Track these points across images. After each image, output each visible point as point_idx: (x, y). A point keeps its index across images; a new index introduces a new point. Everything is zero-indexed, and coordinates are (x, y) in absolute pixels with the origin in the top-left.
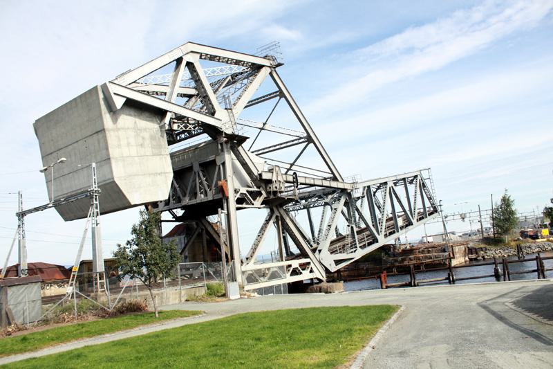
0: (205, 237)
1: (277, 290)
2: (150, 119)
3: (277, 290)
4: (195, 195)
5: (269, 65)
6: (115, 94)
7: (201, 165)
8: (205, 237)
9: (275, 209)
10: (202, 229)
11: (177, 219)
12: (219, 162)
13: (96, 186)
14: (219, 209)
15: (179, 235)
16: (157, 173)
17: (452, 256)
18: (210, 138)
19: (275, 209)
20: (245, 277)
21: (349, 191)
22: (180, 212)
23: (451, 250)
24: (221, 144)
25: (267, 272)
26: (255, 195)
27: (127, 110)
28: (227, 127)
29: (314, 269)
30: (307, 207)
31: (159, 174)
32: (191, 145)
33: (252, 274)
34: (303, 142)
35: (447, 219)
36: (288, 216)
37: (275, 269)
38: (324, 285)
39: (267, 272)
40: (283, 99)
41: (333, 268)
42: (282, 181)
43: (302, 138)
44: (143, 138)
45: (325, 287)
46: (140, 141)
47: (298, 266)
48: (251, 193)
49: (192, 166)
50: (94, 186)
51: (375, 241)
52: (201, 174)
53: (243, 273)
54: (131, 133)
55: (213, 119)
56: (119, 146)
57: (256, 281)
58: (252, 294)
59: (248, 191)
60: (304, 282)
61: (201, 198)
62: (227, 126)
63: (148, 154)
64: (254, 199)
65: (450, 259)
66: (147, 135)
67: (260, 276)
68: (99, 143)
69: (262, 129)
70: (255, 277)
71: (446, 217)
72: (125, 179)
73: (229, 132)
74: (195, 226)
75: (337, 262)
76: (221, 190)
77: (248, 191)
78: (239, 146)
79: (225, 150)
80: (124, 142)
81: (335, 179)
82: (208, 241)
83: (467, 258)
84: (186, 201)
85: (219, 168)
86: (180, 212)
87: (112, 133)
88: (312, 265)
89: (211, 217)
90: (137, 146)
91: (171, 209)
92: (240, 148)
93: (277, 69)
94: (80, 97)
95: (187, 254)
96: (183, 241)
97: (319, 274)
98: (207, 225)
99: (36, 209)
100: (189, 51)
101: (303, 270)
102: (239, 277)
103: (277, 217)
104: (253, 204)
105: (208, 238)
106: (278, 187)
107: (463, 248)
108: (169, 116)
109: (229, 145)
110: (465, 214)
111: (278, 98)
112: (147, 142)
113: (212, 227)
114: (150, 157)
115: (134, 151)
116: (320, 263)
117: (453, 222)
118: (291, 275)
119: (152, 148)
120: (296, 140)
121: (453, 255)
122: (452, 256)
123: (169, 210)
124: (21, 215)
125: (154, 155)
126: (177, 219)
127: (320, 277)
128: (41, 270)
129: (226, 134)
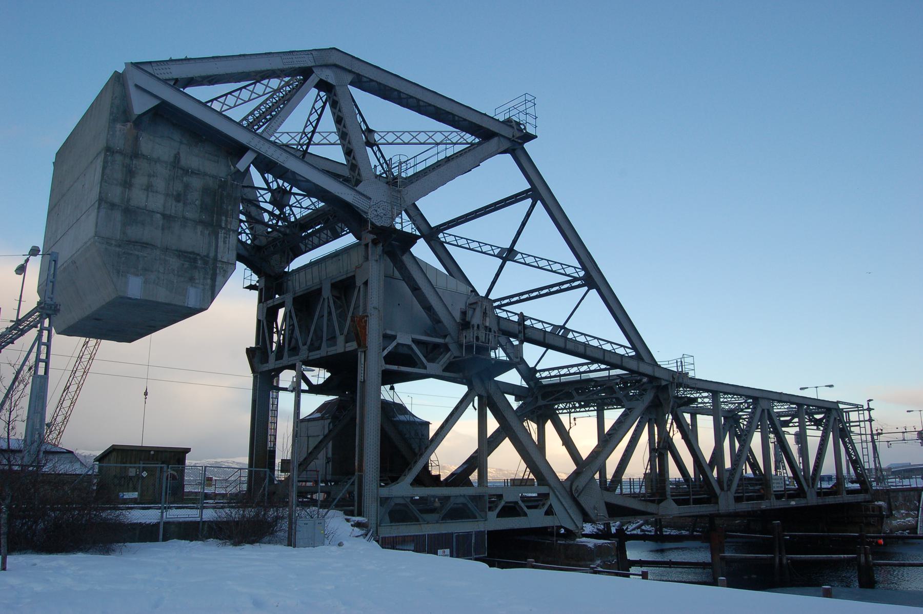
5: (510, 136)
6: (137, 86)
12: (359, 282)
21: (664, 383)
28: (380, 211)
29: (557, 507)
36: (297, 293)
37: (462, 500)
46: (179, 187)
52: (331, 302)
53: (383, 501)
55: (353, 193)
63: (188, 215)
67: (422, 511)
77: (414, 341)
80: (140, 180)
88: (552, 500)
90: (167, 195)
92: (405, 258)
101: (529, 507)
109: (380, 248)
112: (195, 196)
118: (500, 515)
125: (201, 222)
128: (284, 71)
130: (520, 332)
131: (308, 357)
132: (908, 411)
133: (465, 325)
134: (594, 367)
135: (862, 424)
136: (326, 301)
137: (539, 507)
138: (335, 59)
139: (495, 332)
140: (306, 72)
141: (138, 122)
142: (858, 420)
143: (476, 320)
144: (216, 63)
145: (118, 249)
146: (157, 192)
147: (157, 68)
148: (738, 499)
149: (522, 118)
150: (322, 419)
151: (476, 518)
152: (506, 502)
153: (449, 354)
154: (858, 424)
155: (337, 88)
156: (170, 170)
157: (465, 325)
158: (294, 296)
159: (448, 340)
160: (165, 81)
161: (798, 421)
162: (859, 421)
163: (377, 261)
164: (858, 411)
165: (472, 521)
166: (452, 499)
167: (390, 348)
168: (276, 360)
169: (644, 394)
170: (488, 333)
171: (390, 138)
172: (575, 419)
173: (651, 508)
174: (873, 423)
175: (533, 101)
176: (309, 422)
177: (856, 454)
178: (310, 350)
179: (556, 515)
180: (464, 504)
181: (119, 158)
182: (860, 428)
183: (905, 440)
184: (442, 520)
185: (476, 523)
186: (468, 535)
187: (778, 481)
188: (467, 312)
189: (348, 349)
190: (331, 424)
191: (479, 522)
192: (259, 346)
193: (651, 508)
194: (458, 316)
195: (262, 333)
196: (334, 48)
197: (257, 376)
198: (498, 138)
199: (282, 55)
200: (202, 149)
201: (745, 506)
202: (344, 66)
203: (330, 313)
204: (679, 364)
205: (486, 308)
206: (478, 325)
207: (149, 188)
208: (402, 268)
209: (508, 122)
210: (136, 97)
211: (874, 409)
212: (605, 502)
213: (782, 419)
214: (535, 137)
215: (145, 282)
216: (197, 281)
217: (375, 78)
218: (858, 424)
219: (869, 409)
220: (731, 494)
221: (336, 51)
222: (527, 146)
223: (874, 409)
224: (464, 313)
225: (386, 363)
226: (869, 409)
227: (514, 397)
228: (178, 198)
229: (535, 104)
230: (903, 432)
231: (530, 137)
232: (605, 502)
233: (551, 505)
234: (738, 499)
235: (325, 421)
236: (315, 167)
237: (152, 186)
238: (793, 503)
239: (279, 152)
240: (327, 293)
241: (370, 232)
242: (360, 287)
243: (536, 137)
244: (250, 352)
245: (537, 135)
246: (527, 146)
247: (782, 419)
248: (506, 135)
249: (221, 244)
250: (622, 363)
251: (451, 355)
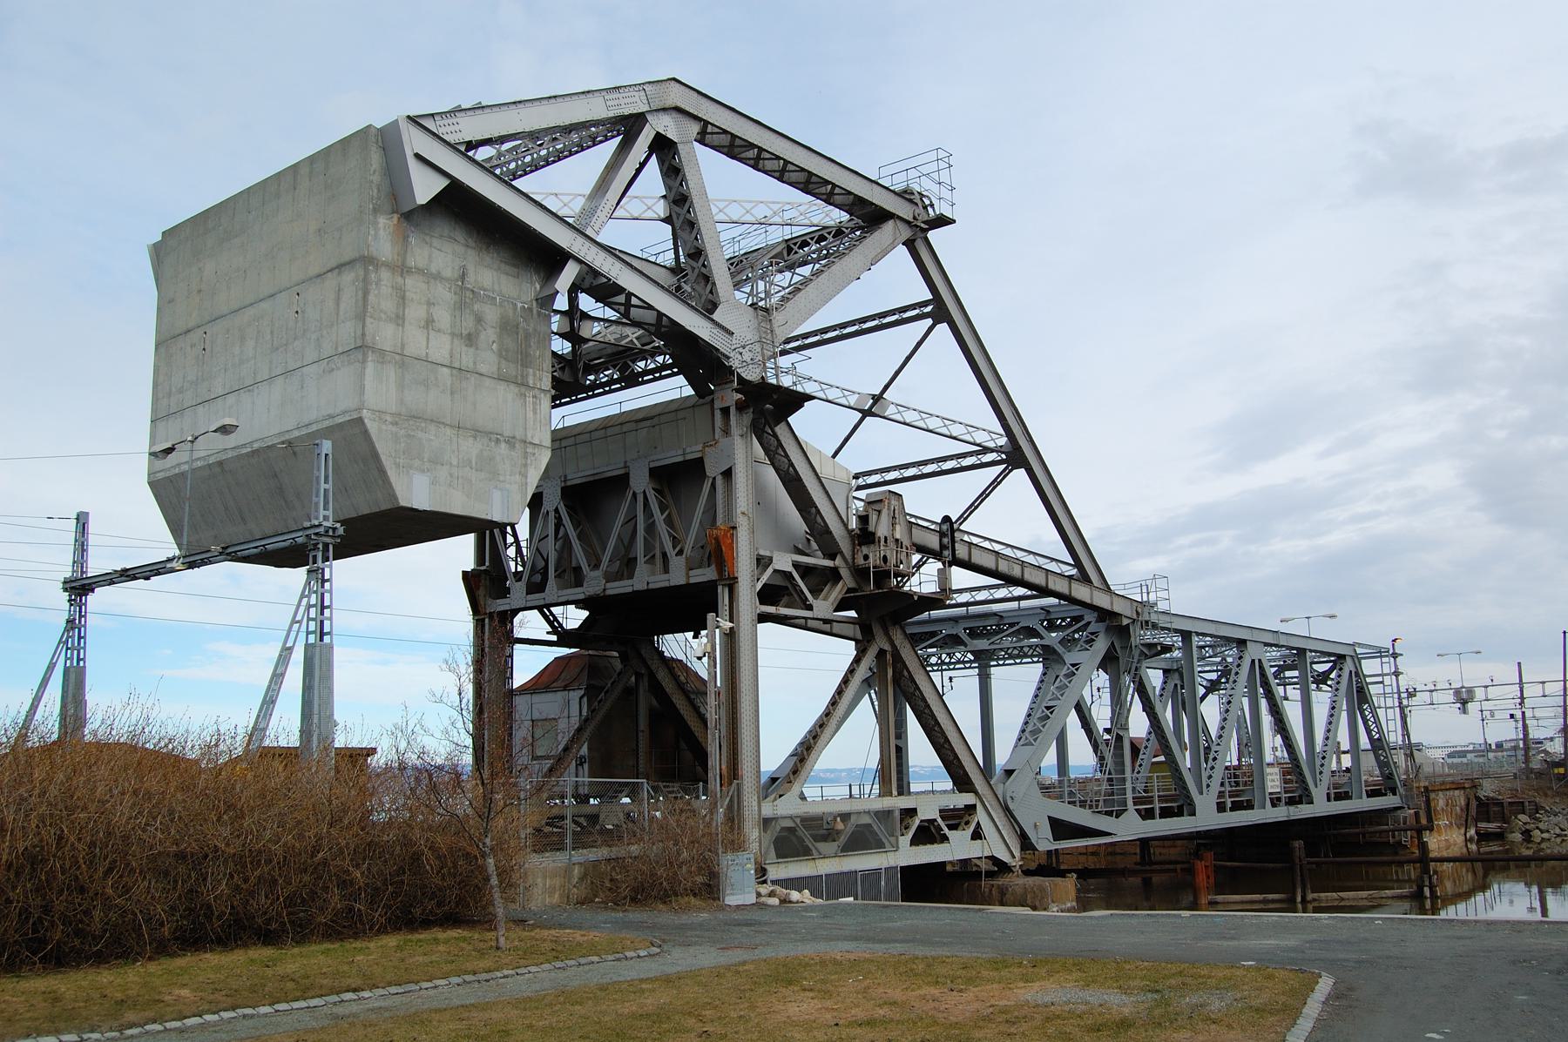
0: (645, 702)
2: (514, 270)
4: (628, 566)
6: (418, 156)
7: (656, 473)
8: (645, 702)
9: (877, 630)
10: (638, 676)
11: (564, 637)
12: (713, 469)
13: (330, 513)
14: (711, 616)
15: (565, 688)
17: (1424, 821)
19: (877, 630)
20: (768, 838)
21: (1125, 622)
22: (573, 617)
23: (1421, 802)
24: (725, 411)
25: (840, 826)
26: (820, 579)
30: (984, 660)
33: (791, 830)
35: (1414, 701)
37: (866, 820)
38: (1017, 882)
39: (840, 826)
40: (943, 328)
41: (1044, 842)
42: (906, 542)
43: (992, 450)
44: (479, 319)
45: (1019, 891)
46: (468, 324)
48: (804, 571)
50: (322, 513)
51: (1181, 805)
53: (766, 822)
54: (444, 293)
56: (399, 320)
57: (801, 852)
58: (795, 895)
59: (796, 565)
60: (949, 868)
61: (644, 578)
62: (747, 356)
63: (483, 368)
64: (816, 592)
65: (1419, 831)
66: (491, 314)
67: (817, 838)
69: (866, 413)
70: (801, 841)
71: (1411, 695)
73: (751, 375)
74: (618, 665)
75: (1061, 829)
76: (718, 553)
77: (796, 565)
78: (777, 423)
79: (735, 430)
80: (415, 312)
81: (1084, 578)
82: (654, 716)
83: (1472, 832)
84: (595, 583)
85: (713, 485)
86: (573, 617)
87: (385, 275)
88: (981, 815)
89: (669, 637)
90: (453, 335)
91: (548, 606)
92: (780, 430)
93: (932, 235)
94: (312, 159)
95: (584, 750)
97: (998, 845)
98: (655, 664)
99: (127, 575)
101: (951, 827)
102: (752, 833)
103: (882, 653)
104: (810, 608)
105: (655, 702)
106: (892, 561)
107: (1460, 798)
108: (570, 273)
109: (748, 417)
110: (1470, 691)
111: (929, 322)
112: (489, 335)
115: (440, 347)
116: (1007, 811)
117: (1429, 711)
118: (915, 841)
119: (500, 356)
120: (971, 454)
121: (1430, 819)
122: (1424, 821)
124: (79, 588)
125: (501, 378)
126: (564, 637)
127: (1004, 856)
129: (741, 380)
131: (604, 590)
132: (82, 521)
133: (865, 536)
134: (1002, 593)
135: (1387, 680)
136: (640, 499)
137: (960, 828)
139: (907, 549)
142: (1380, 673)
143: (882, 530)
144: (517, 111)
145: (394, 429)
146: (439, 331)
147: (441, 123)
148: (1221, 808)
150: (565, 690)
151: (885, 848)
152: (922, 821)
153: (841, 584)
154: (1380, 679)
155: (680, 147)
156: (455, 294)
157: (865, 536)
158: (563, 484)
159: (838, 562)
160: (453, 147)
161: (1297, 675)
162: (1382, 675)
163: (742, 436)
164: (1381, 657)
165: (797, 861)
166: (853, 818)
167: (765, 578)
168: (527, 594)
169: (1094, 640)
170: (899, 549)
172: (951, 679)
174: (1400, 677)
175: (946, 160)
176: (534, 695)
177: (1380, 730)
178: (609, 578)
179: (985, 838)
182: (1384, 686)
183: (1433, 704)
184: (841, 852)
185: (884, 855)
187: (1273, 777)
188: (870, 516)
189: (692, 581)
190: (585, 699)
191: (888, 854)
192: (483, 568)
194: (853, 523)
195: (1260, 673)
196: (674, 79)
197: (483, 620)
198: (892, 220)
199: (604, 93)
200: (495, 255)
202: (687, 109)
203: (651, 528)
204: (1144, 590)
205: (894, 510)
206: (886, 538)
207: (429, 323)
209: (906, 195)
210: (418, 174)
211: (1402, 655)
212: (1049, 817)
213: (488, 532)
214: (950, 221)
215: (434, 482)
216: (501, 478)
217: (723, 124)
218: (1380, 679)
219: (1395, 655)
221: (678, 85)
223: (1402, 655)
224: (864, 519)
225: (762, 603)
226: (1395, 655)
227: (574, 606)
228: (470, 339)
229: (950, 166)
230: (1431, 691)
231: (942, 221)
232: (1049, 817)
233: (978, 822)
235: (571, 692)
236: (658, 284)
237: (433, 321)
241: (737, 391)
242: (714, 478)
243: (954, 221)
244: (465, 574)
245: (954, 218)
246: (933, 235)
247: (488, 532)
248: (905, 217)
249: (530, 414)
250: (1070, 592)
251: (843, 586)
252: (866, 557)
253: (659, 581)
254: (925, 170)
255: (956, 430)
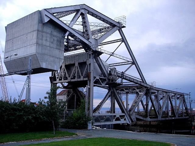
1: (108, 127)
3: (108, 127)
6: (46, 15)
9: (111, 88)
11: (64, 87)
16: (56, 57)
18: (85, 51)
19: (111, 88)
21: (149, 88)
22: (66, 84)
25: (104, 117)
26: (103, 80)
27: (49, 25)
28: (94, 46)
29: (126, 119)
31: (57, 58)
32: (75, 53)
33: (97, 118)
34: (130, 64)
37: (108, 117)
39: (104, 117)
44: (54, 40)
47: (119, 116)
48: (101, 79)
49: (75, 63)
59: (99, 78)
63: (54, 47)
66: (56, 39)
68: (33, 36)
69: (111, 55)
72: (41, 55)
76: (88, 75)
77: (99, 78)
80: (44, 38)
88: (126, 117)
90: (50, 42)
92: (98, 58)
96: (65, 98)
98: (77, 92)
100: (83, 8)
103: (112, 92)
108: (67, 33)
109: (93, 56)
112: (55, 42)
113: (80, 93)
114: (55, 49)
118: (115, 120)
119: (57, 45)
120: (127, 62)
123: (61, 83)
126: (64, 87)
130: (122, 76)
135: (188, 99)
136: (77, 67)
138: (84, 7)
140: (78, 11)
141: (44, 24)
148: (162, 117)
149: (122, 21)
159: (106, 78)
171: (93, 24)
173: (145, 119)
178: (71, 79)
180: (108, 118)
181: (40, 33)
186: (109, 125)
193: (145, 119)
201: (163, 119)
207: (46, 40)
208: (97, 61)
209: (119, 23)
220: (161, 116)
222: (122, 29)
228: (52, 43)
231: (124, 27)
232: (136, 118)
234: (162, 117)
236: (79, 34)
238: (173, 118)
239: (71, 30)
240: (77, 64)
241: (92, 52)
246: (122, 29)
249: (61, 54)
252: (110, 77)
253: (79, 80)
254: (121, 19)
255: (124, 58)
